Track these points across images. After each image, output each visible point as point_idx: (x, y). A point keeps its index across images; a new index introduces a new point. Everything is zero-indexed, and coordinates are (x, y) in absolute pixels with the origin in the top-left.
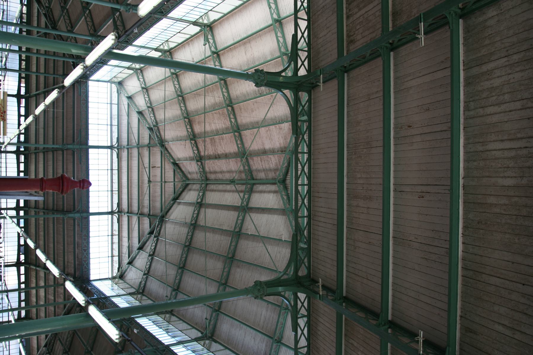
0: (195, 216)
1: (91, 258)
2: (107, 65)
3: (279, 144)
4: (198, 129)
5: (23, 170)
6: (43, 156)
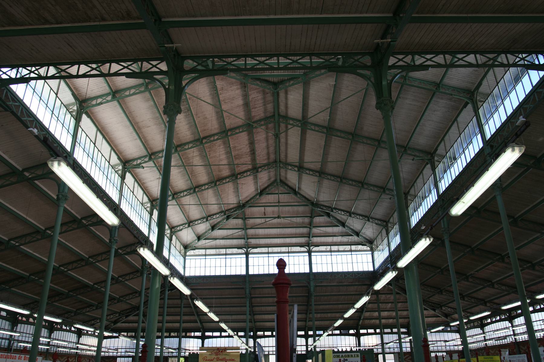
0: (311, 173)
2: (169, 260)
3: (237, 89)
4: (226, 172)
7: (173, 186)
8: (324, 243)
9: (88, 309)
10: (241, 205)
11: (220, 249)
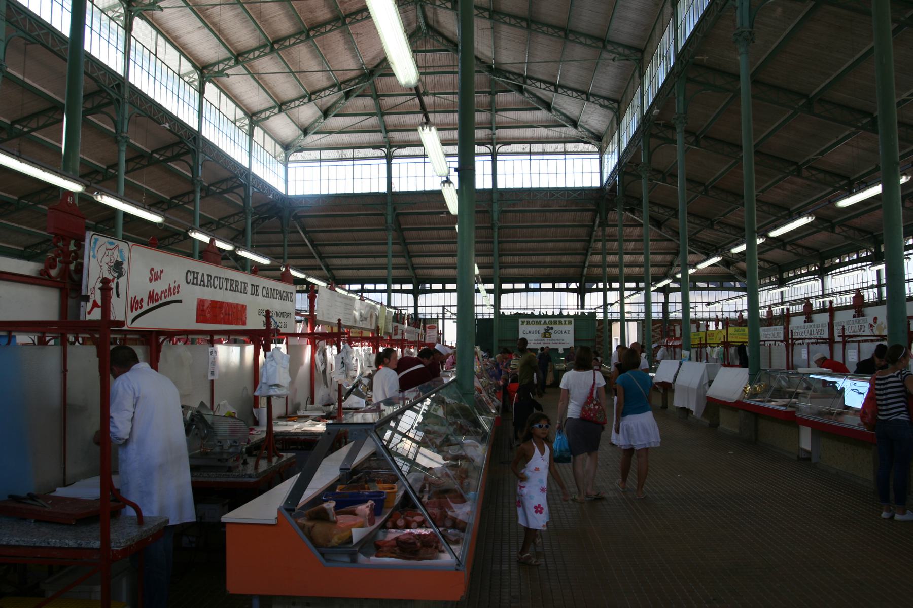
1: (556, 186)
2: (249, 169)
5: (441, 285)
6: (417, 258)
7: (233, 41)
8: (519, 139)
9: (172, 240)
10: (365, 73)
11: (344, 150)
